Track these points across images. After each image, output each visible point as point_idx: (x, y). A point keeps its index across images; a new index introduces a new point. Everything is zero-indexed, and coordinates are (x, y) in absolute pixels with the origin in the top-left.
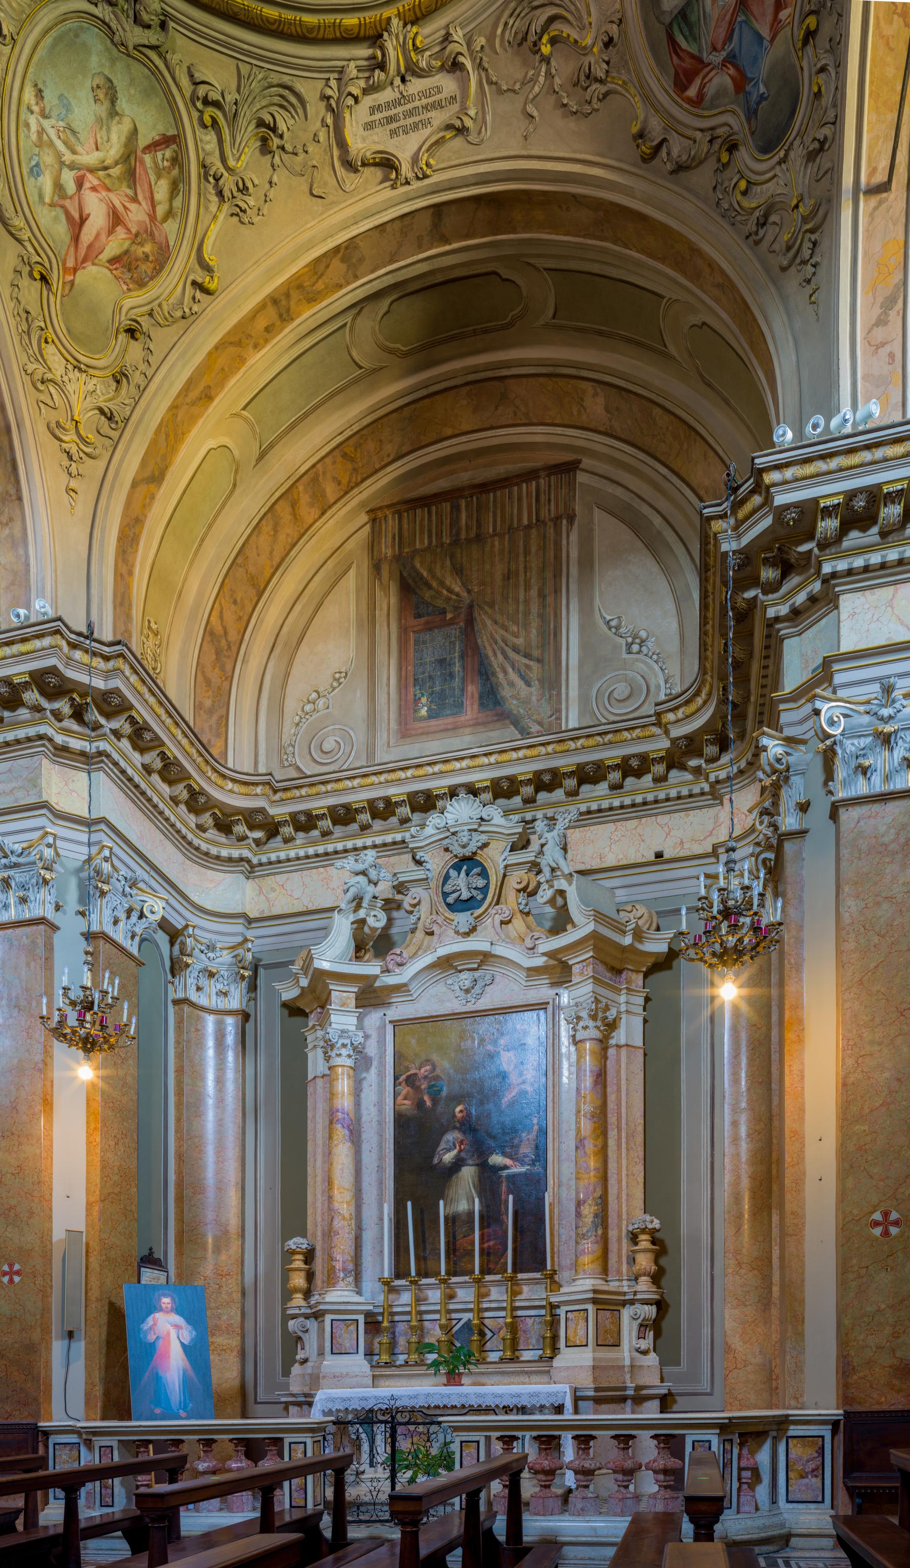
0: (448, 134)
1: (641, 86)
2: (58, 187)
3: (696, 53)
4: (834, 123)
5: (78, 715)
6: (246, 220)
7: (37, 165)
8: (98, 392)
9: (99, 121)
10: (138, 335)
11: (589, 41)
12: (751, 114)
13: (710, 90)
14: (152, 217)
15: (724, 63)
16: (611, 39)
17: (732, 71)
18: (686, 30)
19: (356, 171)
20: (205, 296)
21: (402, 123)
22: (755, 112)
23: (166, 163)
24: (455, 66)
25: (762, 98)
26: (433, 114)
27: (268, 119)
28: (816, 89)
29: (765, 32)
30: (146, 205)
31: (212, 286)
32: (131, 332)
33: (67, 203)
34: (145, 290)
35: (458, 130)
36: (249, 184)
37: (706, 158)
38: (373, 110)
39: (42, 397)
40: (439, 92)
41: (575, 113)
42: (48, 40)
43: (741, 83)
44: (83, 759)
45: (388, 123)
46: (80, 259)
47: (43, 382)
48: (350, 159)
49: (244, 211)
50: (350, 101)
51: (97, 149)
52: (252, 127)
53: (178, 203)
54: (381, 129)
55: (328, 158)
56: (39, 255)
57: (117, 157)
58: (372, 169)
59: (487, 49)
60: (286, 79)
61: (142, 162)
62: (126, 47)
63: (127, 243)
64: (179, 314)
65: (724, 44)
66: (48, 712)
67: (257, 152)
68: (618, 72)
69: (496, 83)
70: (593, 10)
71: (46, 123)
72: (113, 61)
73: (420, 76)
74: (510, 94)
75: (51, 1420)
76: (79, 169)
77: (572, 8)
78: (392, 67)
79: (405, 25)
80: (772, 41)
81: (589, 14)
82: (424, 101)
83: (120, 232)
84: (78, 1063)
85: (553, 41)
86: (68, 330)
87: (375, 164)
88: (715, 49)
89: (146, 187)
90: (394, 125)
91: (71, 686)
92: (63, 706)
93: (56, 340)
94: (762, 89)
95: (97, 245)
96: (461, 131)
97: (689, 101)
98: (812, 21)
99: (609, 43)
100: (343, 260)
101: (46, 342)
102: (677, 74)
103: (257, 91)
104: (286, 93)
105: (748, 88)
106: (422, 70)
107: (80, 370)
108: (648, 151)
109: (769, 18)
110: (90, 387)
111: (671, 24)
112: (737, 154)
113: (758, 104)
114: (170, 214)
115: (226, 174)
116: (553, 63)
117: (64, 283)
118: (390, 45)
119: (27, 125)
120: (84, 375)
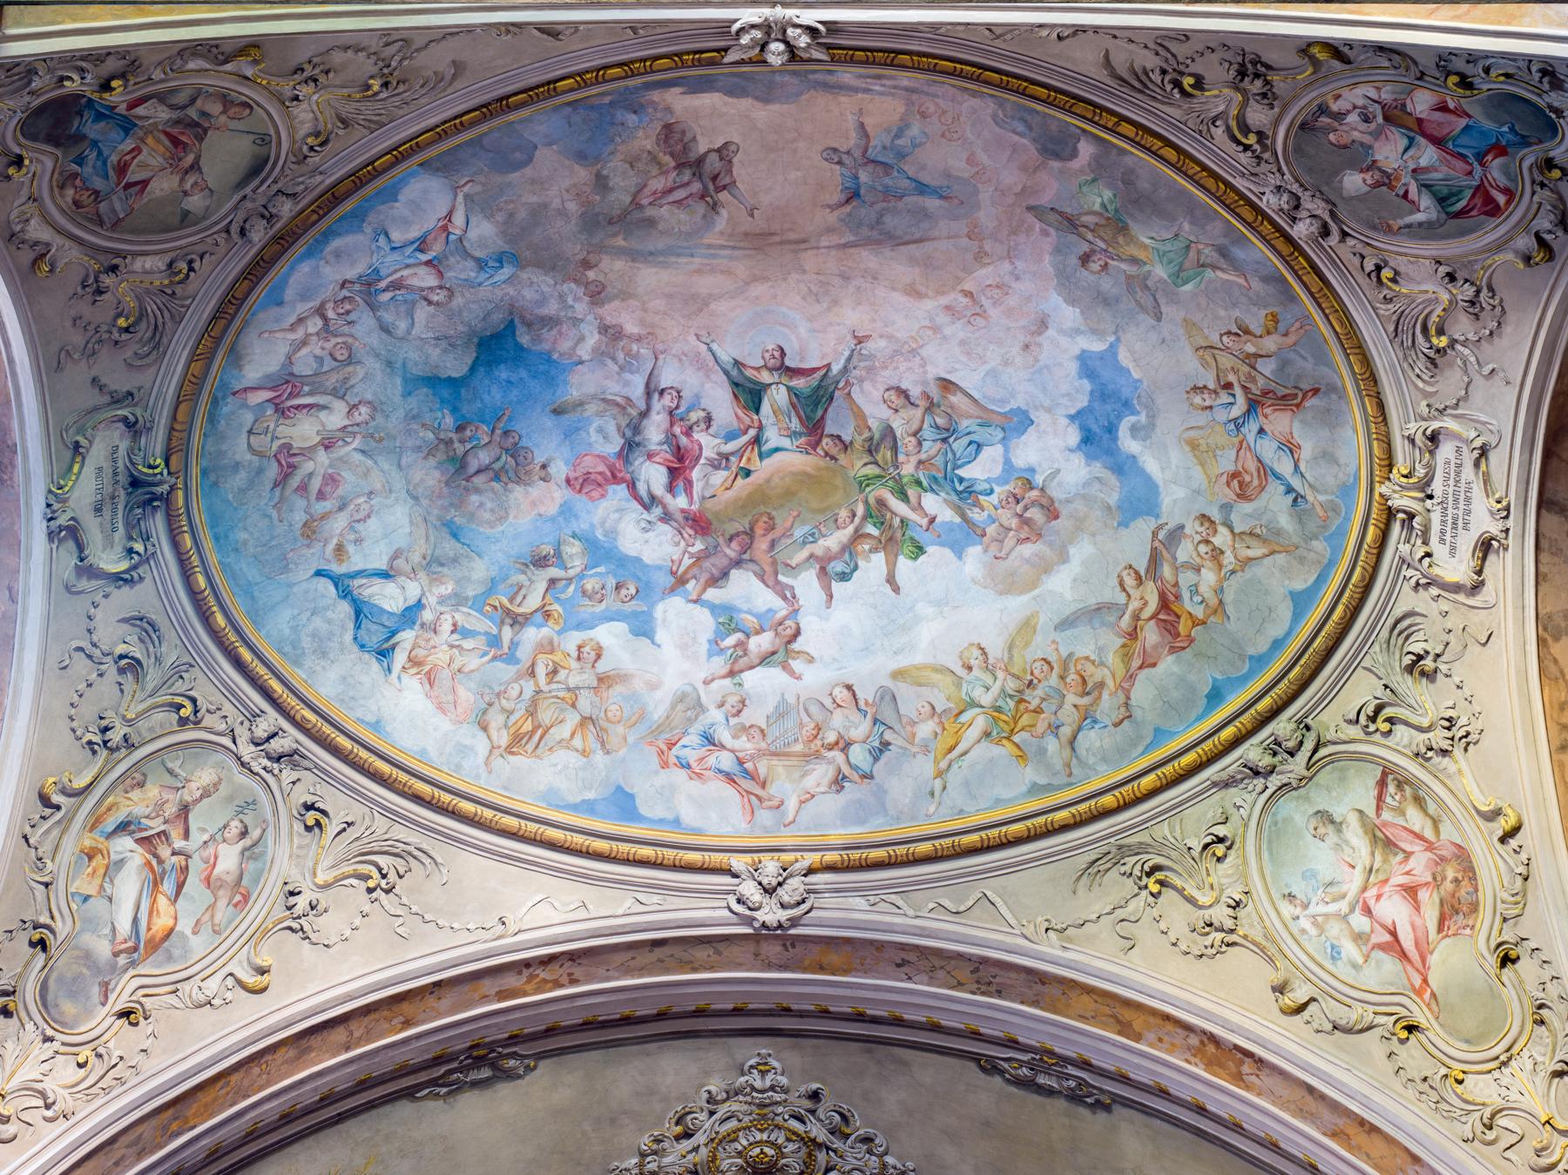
0: (1483, 467)
1: (1490, 251)
2: (1359, 938)
3: (1471, 191)
4: (1530, 61)
6: (1477, 736)
7: (1333, 947)
8: (1539, 1059)
9: (1337, 847)
10: (1513, 954)
11: (1445, 297)
12: (1525, 142)
13: (1503, 181)
14: (1430, 847)
15: (1482, 165)
16: (1448, 274)
17: (1489, 157)
18: (1453, 199)
19: (1482, 583)
20: (1519, 836)
21: (1460, 513)
22: (1523, 137)
23: (1397, 798)
24: (1434, 438)
25: (1512, 129)
26: (1463, 477)
27: (1408, 660)
28: (1502, 78)
29: (1463, 122)
30: (1417, 847)
31: (1512, 821)
32: (1506, 960)
33: (1375, 939)
34: (1481, 908)
35: (1481, 455)
36: (1450, 713)
37: (1558, 193)
38: (1442, 541)
39: (1503, 1144)
40: (1449, 463)
41: (1499, 324)
42: (1266, 855)
43: (1500, 150)
45: (1456, 529)
46: (1419, 965)
47: (1490, 1128)
48: (1469, 586)
49: (1468, 735)
50: (1427, 561)
51: (1353, 867)
52: (1409, 679)
53: (1432, 807)
54: (1458, 538)
55: (1463, 609)
56: (1392, 1014)
57: (1369, 849)
58: (1487, 563)
59: (1431, 401)
60: (1391, 621)
61: (1385, 824)
62: (1304, 778)
63: (1435, 894)
64: (1519, 880)
65: (1468, 163)
67: (1431, 686)
68: (1475, 271)
69: (1459, 400)
70: (1424, 288)
71: (1312, 910)
72: (1307, 798)
73: (1432, 479)
74: (1470, 389)
76: (1358, 902)
77: (1421, 307)
78: (1415, 506)
79: (1389, 479)
80: (1469, 116)
81: (1427, 292)
82: (1451, 482)
83: (1423, 895)
85: (1441, 332)
86: (1467, 1041)
87: (1484, 559)
88: (1470, 173)
89: (1404, 834)
90: (1460, 524)
93: (1466, 1067)
94: (1505, 129)
95: (1420, 934)
96: (1484, 452)
97: (1508, 203)
98: (1453, 79)
99: (1451, 277)
100: (1557, 639)
101: (1460, 1082)
102: (1486, 213)
103: (1386, 658)
104: (1400, 627)
105: (1504, 143)
106: (1427, 474)
107: (1504, 1064)
108: (1542, 254)
109: (1452, 118)
110: (1529, 1065)
111: (1447, 213)
112: (1557, 161)
113: (1517, 134)
114: (1436, 823)
115: (1430, 735)
116: (1456, 337)
117: (1428, 1005)
118: (1397, 502)
119: (1303, 931)
120: (1513, 1063)
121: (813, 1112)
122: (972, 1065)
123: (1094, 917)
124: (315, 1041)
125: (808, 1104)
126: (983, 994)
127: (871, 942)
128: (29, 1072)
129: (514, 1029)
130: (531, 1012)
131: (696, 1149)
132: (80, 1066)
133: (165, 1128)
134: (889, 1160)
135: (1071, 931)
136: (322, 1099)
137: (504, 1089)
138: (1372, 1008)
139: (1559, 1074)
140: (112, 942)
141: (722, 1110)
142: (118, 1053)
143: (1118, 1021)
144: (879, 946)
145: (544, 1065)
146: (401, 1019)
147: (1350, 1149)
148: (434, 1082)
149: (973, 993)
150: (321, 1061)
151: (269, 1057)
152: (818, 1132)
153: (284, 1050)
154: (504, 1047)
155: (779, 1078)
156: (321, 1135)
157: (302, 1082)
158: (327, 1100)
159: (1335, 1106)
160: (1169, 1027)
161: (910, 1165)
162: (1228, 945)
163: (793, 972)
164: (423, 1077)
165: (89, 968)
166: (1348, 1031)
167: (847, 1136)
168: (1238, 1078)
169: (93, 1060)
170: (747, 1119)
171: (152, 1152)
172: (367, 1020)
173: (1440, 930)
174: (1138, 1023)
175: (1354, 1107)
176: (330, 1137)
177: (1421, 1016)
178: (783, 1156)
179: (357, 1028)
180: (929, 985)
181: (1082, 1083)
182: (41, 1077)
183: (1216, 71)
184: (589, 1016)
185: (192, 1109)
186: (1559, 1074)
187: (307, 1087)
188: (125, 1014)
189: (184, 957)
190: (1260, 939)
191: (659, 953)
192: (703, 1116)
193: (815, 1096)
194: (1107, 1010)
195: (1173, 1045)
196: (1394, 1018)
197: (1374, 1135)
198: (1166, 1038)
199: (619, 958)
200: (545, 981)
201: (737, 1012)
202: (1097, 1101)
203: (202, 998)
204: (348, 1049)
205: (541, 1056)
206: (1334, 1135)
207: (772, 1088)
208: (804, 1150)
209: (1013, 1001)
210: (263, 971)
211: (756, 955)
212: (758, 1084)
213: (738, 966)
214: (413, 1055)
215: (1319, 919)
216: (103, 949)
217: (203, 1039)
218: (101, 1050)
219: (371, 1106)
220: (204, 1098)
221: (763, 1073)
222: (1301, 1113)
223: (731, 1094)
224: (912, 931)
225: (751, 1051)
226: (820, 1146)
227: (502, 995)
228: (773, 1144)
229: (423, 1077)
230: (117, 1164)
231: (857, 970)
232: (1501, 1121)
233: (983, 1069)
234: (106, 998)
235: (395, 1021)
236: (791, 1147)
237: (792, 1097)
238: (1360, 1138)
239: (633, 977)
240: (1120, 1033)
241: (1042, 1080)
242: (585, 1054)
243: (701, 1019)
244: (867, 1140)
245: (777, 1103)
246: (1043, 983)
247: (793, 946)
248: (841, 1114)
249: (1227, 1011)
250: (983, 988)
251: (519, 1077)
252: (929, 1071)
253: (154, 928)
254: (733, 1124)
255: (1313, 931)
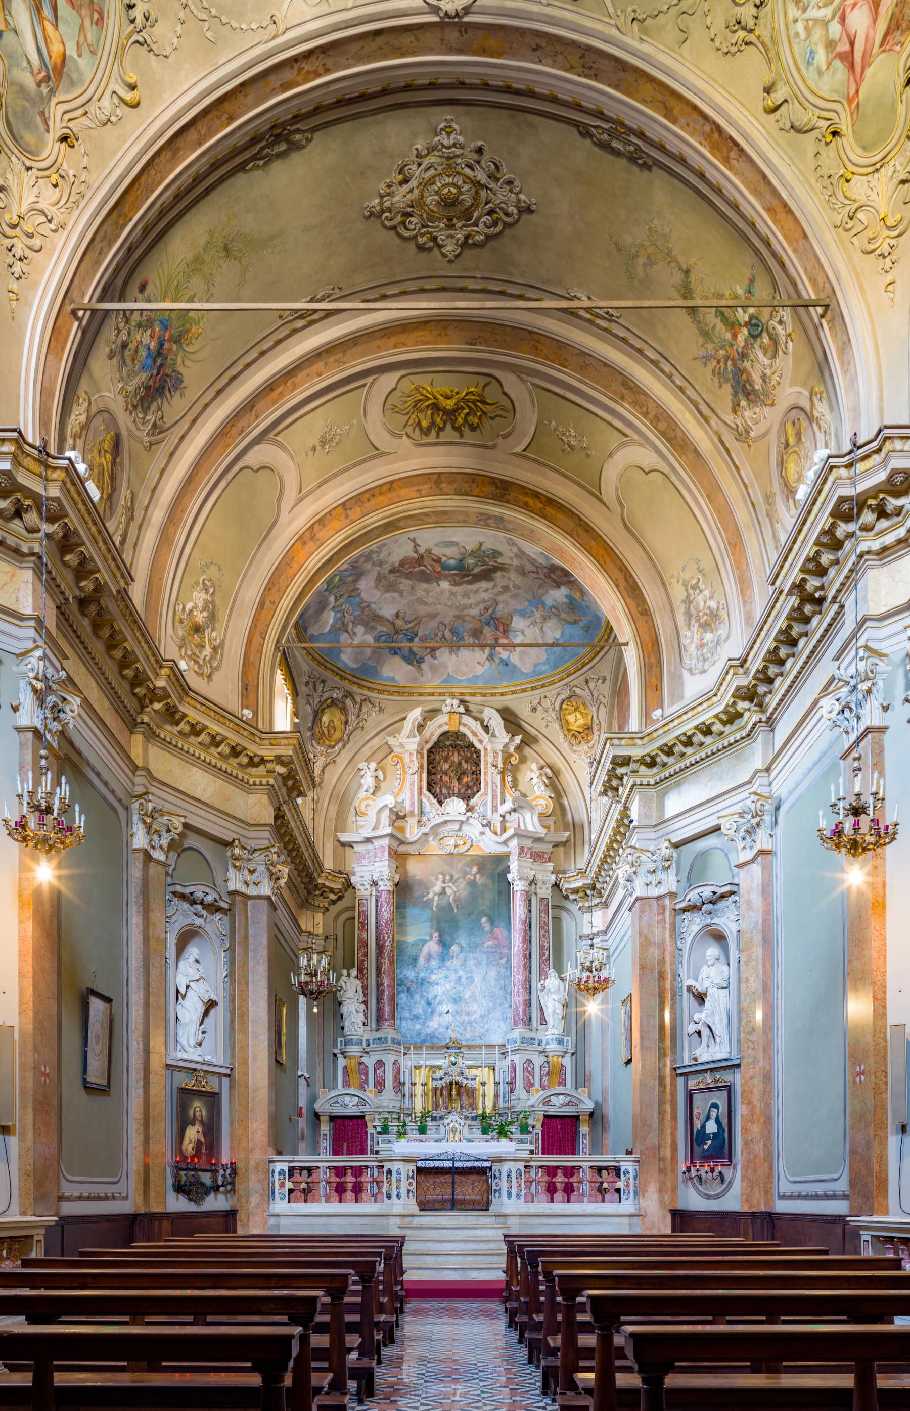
5: (882, 513)
39: (854, 232)
44: (902, 545)
66: (858, 532)
75: (886, 1213)
84: (843, 870)
91: (863, 498)
92: (868, 517)
117: (852, 114)
119: (797, 35)
120: (883, 170)
121: (478, 162)
122: (574, 130)
123: (665, 8)
124: (180, 142)
125: (475, 156)
126: (586, 76)
127: (517, 29)
128: (28, 198)
129: (295, 111)
130: (304, 99)
131: (411, 191)
132: (55, 186)
133: (116, 224)
134: (522, 196)
135: (649, 22)
136: (194, 181)
137: (296, 157)
138: (818, 112)
139: (903, 182)
140: (32, 72)
141: (426, 162)
142: (71, 172)
143: (666, 107)
144: (522, 32)
145: (317, 136)
146: (226, 116)
147: (774, 221)
148: (255, 158)
149: (580, 75)
150: (188, 157)
151: (157, 161)
152: (482, 177)
153: (164, 153)
154: (291, 125)
155: (459, 137)
156: (200, 205)
157: (180, 174)
158: (197, 180)
159: (774, 192)
160: (695, 116)
161: (534, 200)
162: (746, 44)
163: (466, 54)
164: (247, 154)
165: (27, 100)
166: (798, 131)
167: (498, 180)
168: (726, 161)
169: (60, 181)
170: (440, 168)
171: (115, 241)
172: (206, 120)
173: (882, 45)
174: (678, 108)
175: (784, 195)
176: (204, 205)
177: (845, 126)
178: (461, 193)
179: (202, 127)
180: (552, 67)
181: (638, 148)
182: (36, 199)
183: (650, 416)
184: (339, 95)
185: (127, 207)
186: (903, 182)
187: (184, 177)
188: (64, 139)
189: (81, 81)
190: (767, 40)
191: (380, 40)
192: (414, 167)
193: (480, 151)
194: (660, 97)
195: (695, 129)
196: (829, 123)
197: (789, 216)
198: (691, 123)
199: (354, 47)
200: (309, 72)
201: (432, 86)
202: (645, 163)
203: (104, 118)
204: (200, 144)
205: (314, 130)
206: (768, 210)
207: (454, 145)
208: (474, 189)
209: (603, 83)
210: (133, 87)
211: (442, 40)
212: (446, 142)
213: (430, 51)
214: (240, 139)
215: (810, 23)
216: (29, 82)
217: (115, 153)
218: (63, 173)
219: (222, 180)
220: (131, 198)
221: (449, 134)
222: (756, 192)
223: (431, 149)
224: (544, 19)
225: (442, 116)
226: (483, 186)
227: (285, 87)
228: (455, 185)
229: (247, 154)
230: (100, 253)
231: (507, 53)
232: (860, 215)
233: (581, 133)
234: (48, 126)
235: (223, 118)
236: (466, 187)
237: (466, 151)
238: (781, 215)
239: (364, 64)
240: (665, 116)
241: (615, 144)
242: (340, 126)
243: (409, 93)
244: (510, 183)
245: (457, 156)
246: (624, 71)
247: (466, 32)
248: (495, 164)
249: (732, 107)
250: (586, 71)
251: (304, 147)
252: (550, 131)
253: (53, 56)
254: (432, 172)
255: (803, 35)
